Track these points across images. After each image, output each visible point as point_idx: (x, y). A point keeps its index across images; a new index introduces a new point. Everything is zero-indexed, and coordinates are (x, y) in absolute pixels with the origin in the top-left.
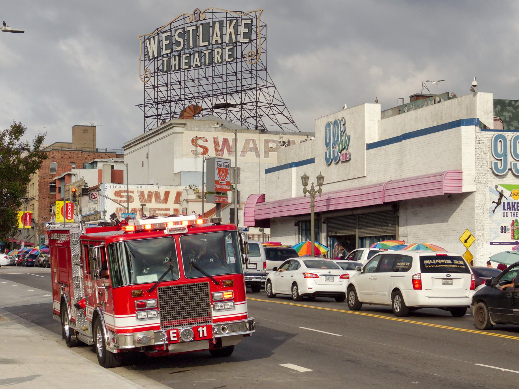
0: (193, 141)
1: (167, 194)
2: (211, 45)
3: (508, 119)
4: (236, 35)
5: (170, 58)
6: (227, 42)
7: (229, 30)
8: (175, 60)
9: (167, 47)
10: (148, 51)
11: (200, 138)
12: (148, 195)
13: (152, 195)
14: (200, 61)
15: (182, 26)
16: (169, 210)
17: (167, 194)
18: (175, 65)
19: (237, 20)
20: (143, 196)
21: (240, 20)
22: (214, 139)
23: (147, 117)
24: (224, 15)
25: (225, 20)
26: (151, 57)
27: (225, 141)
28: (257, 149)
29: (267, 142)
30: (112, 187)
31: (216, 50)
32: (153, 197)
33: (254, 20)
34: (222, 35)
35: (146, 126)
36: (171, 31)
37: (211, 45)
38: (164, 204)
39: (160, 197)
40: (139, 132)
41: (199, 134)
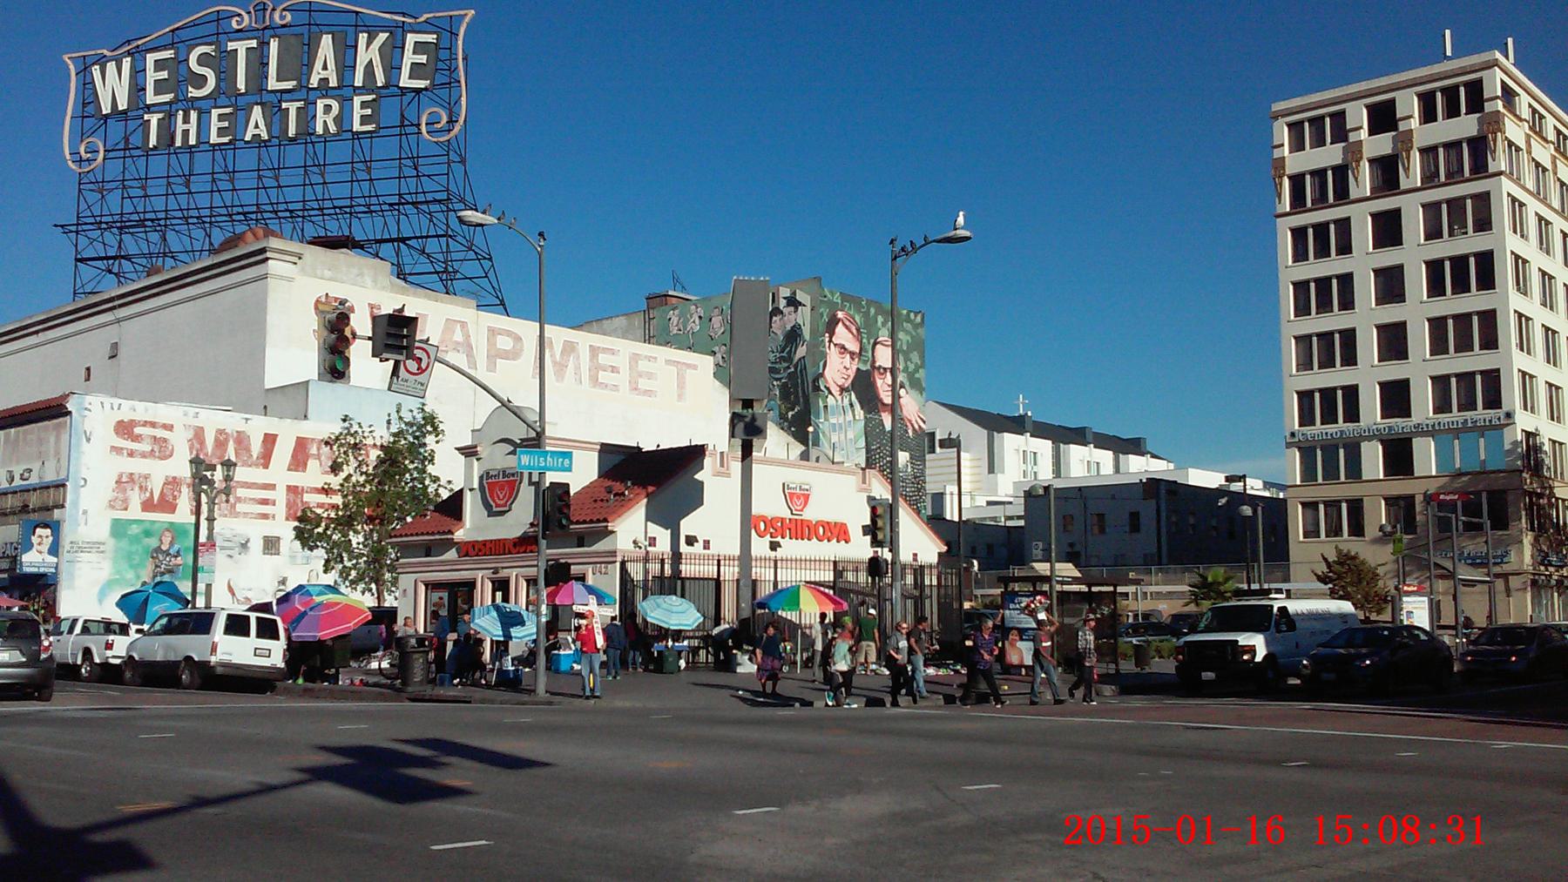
1: (270, 440)
5: (171, 116)
7: (368, 53)
8: (186, 120)
9: (160, 87)
12: (217, 440)
13: (227, 440)
16: (272, 487)
17: (270, 440)
23: (82, 260)
29: (493, 332)
31: (320, 104)
35: (79, 284)
38: (261, 470)
39: (248, 450)
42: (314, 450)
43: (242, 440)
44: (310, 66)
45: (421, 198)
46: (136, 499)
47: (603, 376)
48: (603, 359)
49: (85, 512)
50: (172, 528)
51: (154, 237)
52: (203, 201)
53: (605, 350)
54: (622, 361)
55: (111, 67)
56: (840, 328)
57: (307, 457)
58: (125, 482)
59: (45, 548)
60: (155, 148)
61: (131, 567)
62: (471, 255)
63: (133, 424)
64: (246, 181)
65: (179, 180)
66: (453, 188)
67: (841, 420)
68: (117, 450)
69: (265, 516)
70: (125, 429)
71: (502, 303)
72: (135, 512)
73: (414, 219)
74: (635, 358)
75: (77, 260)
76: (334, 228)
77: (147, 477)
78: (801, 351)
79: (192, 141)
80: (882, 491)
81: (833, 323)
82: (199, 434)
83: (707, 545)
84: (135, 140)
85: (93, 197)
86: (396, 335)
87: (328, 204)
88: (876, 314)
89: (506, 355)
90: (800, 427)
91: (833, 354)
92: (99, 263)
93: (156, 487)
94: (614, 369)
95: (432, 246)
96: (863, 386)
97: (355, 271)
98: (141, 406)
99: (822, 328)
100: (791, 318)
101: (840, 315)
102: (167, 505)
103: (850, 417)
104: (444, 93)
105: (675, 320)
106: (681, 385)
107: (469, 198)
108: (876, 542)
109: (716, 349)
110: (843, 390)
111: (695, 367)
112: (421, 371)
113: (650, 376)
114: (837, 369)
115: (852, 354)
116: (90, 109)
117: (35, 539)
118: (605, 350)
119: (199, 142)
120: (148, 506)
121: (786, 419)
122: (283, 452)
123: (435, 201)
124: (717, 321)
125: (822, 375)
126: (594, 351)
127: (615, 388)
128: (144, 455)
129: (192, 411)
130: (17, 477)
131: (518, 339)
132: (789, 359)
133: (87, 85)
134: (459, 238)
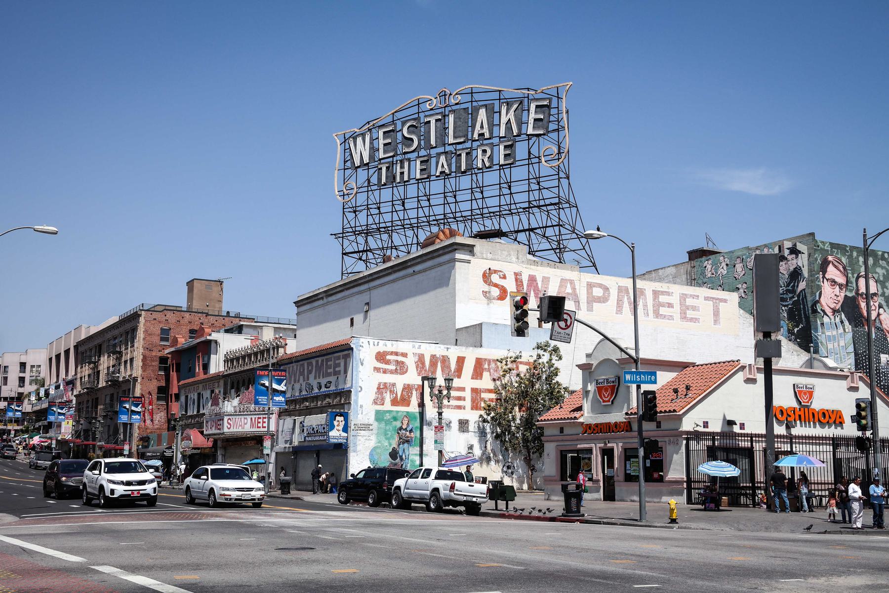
0: (484, 275)
1: (461, 361)
2: (470, 142)
3: (881, 279)
4: (520, 123)
6: (502, 134)
7: (507, 116)
8: (402, 167)
10: (351, 155)
11: (495, 272)
12: (431, 361)
14: (449, 165)
15: (416, 116)
17: (461, 361)
18: (402, 173)
19: (521, 103)
20: (423, 364)
21: (526, 103)
22: (516, 274)
24: (496, 95)
25: (497, 103)
26: (357, 163)
27: (532, 279)
28: (576, 295)
29: (590, 286)
30: (371, 344)
32: (439, 364)
33: (555, 100)
34: (491, 126)
36: (395, 125)
37: (470, 142)
39: (449, 367)
40: (334, 279)
41: (495, 265)
42: (486, 366)
43: (445, 360)
44: (473, 127)
45: (542, 203)
46: (388, 398)
47: (662, 311)
48: (663, 299)
49: (361, 406)
50: (408, 415)
51: (385, 237)
52: (412, 214)
53: (663, 293)
54: (675, 300)
55: (359, 140)
56: (831, 268)
57: (483, 370)
58: (382, 388)
59: (341, 428)
60: (385, 184)
61: (386, 439)
62: (574, 236)
63: (385, 353)
64: (437, 200)
65: (398, 202)
66: (562, 194)
67: (834, 333)
68: (377, 369)
69: (459, 407)
70: (381, 357)
71: (594, 265)
72: (388, 406)
73: (538, 215)
74: (683, 297)
75: (343, 254)
76: (490, 225)
77: (394, 385)
78: (802, 285)
79: (406, 178)
80: (864, 393)
81: (825, 265)
82: (421, 358)
83: (742, 426)
84: (374, 180)
85: (351, 216)
86: (554, 309)
87: (486, 211)
88: (858, 256)
89: (600, 300)
90: (806, 340)
91: (826, 287)
92: (355, 255)
93: (399, 389)
94: (670, 305)
95: (549, 232)
96: (851, 309)
97: (506, 253)
98: (389, 343)
99: (816, 268)
100: (793, 263)
101: (830, 258)
102: (405, 401)
103: (841, 330)
104: (554, 135)
105: (709, 267)
106: (716, 313)
107: (572, 200)
108: (862, 428)
109: (740, 286)
110: (834, 311)
111: (725, 301)
112: (567, 327)
113: (694, 308)
114: (830, 297)
115: (841, 286)
116: (349, 164)
117: (336, 423)
118: (663, 293)
119: (409, 179)
120: (394, 402)
121: (793, 334)
122: (469, 368)
123: (551, 204)
124: (739, 267)
125: (818, 302)
126: (656, 293)
127: (671, 318)
128: (391, 372)
129: (417, 345)
130: (323, 386)
131: (606, 289)
132: (793, 291)
133: (347, 150)
134: (567, 226)
